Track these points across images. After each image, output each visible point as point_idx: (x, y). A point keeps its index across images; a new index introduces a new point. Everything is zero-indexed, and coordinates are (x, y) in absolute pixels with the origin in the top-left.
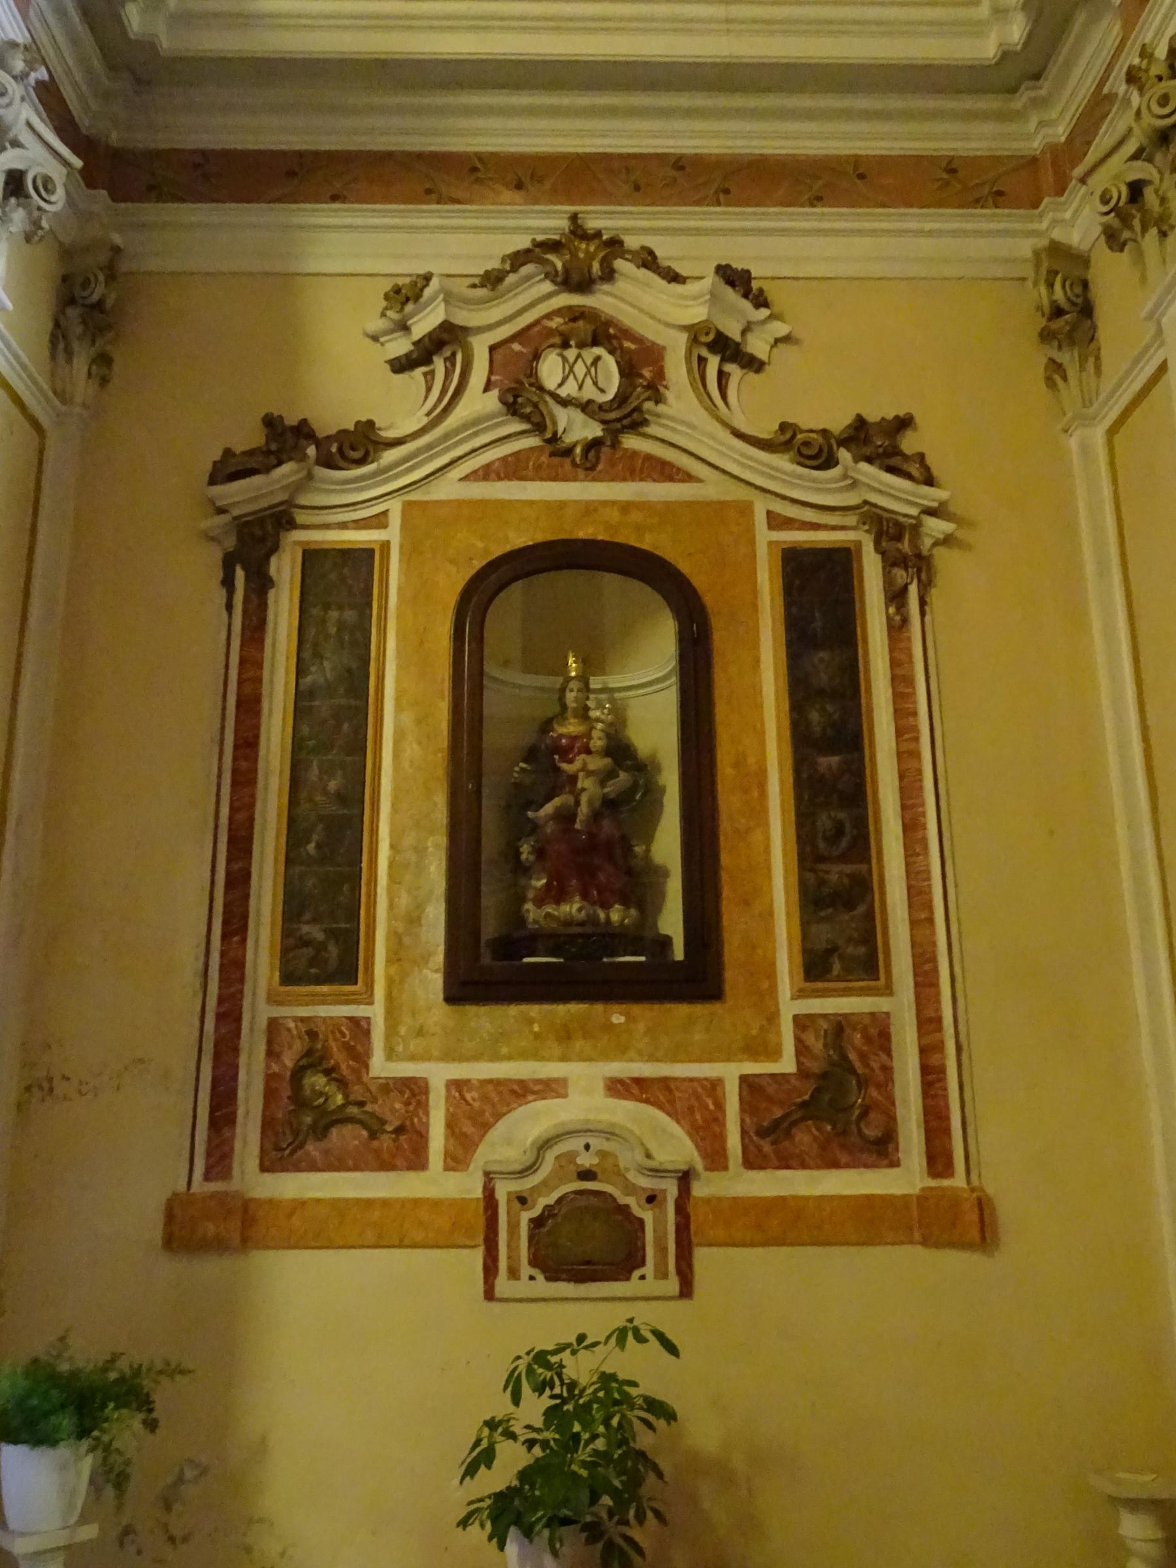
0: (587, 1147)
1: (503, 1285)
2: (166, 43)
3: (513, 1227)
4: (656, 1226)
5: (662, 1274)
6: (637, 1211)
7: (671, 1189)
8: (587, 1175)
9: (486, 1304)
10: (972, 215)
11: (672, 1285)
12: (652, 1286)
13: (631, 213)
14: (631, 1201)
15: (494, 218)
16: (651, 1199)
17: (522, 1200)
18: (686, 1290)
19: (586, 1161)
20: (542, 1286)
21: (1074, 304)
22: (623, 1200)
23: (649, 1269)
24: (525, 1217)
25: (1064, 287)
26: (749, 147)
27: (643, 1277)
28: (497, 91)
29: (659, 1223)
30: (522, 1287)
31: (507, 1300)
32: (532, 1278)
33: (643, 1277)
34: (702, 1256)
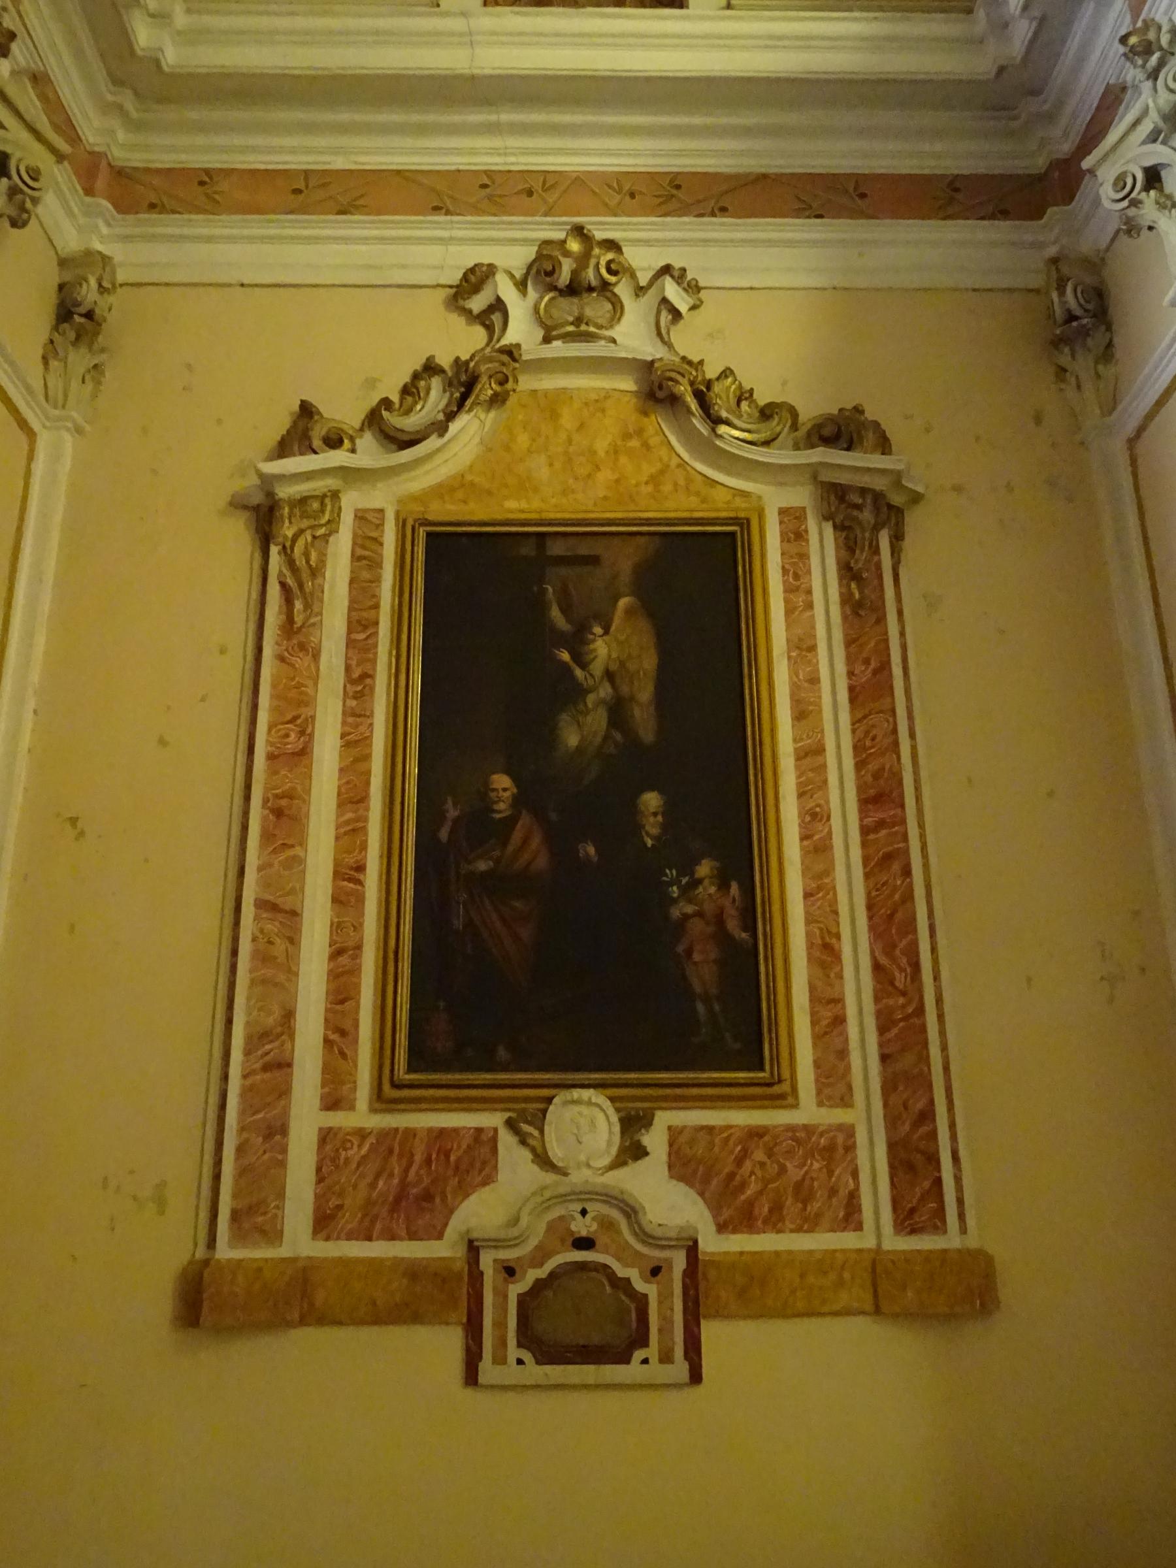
0: (584, 1212)
1: (488, 1371)
2: (171, 57)
3: (501, 1307)
4: (664, 1304)
5: (666, 1358)
6: (640, 1286)
7: (679, 1261)
8: (584, 1243)
9: (469, 1392)
10: (325, 221)
11: (680, 1369)
12: (657, 1372)
13: (393, 222)
14: (633, 1274)
15: (377, 228)
16: (655, 1271)
17: (510, 1271)
18: (696, 1377)
19: (582, 1227)
20: (536, 1372)
21: (1086, 310)
22: (621, 1271)
23: (652, 1351)
24: (516, 1289)
25: (1075, 291)
26: (506, 164)
27: (645, 1361)
28: (891, 76)
29: (665, 1297)
30: (510, 1374)
31: (492, 1387)
32: (520, 1362)
33: (645, 1361)
34: (710, 1331)
